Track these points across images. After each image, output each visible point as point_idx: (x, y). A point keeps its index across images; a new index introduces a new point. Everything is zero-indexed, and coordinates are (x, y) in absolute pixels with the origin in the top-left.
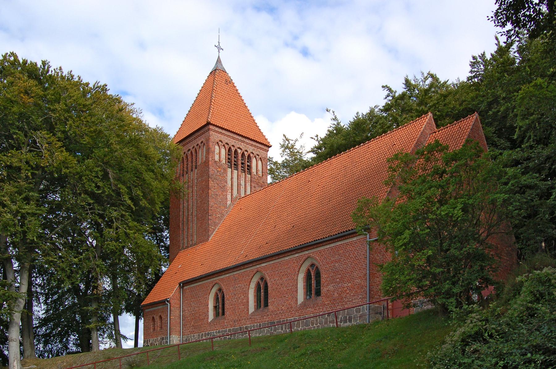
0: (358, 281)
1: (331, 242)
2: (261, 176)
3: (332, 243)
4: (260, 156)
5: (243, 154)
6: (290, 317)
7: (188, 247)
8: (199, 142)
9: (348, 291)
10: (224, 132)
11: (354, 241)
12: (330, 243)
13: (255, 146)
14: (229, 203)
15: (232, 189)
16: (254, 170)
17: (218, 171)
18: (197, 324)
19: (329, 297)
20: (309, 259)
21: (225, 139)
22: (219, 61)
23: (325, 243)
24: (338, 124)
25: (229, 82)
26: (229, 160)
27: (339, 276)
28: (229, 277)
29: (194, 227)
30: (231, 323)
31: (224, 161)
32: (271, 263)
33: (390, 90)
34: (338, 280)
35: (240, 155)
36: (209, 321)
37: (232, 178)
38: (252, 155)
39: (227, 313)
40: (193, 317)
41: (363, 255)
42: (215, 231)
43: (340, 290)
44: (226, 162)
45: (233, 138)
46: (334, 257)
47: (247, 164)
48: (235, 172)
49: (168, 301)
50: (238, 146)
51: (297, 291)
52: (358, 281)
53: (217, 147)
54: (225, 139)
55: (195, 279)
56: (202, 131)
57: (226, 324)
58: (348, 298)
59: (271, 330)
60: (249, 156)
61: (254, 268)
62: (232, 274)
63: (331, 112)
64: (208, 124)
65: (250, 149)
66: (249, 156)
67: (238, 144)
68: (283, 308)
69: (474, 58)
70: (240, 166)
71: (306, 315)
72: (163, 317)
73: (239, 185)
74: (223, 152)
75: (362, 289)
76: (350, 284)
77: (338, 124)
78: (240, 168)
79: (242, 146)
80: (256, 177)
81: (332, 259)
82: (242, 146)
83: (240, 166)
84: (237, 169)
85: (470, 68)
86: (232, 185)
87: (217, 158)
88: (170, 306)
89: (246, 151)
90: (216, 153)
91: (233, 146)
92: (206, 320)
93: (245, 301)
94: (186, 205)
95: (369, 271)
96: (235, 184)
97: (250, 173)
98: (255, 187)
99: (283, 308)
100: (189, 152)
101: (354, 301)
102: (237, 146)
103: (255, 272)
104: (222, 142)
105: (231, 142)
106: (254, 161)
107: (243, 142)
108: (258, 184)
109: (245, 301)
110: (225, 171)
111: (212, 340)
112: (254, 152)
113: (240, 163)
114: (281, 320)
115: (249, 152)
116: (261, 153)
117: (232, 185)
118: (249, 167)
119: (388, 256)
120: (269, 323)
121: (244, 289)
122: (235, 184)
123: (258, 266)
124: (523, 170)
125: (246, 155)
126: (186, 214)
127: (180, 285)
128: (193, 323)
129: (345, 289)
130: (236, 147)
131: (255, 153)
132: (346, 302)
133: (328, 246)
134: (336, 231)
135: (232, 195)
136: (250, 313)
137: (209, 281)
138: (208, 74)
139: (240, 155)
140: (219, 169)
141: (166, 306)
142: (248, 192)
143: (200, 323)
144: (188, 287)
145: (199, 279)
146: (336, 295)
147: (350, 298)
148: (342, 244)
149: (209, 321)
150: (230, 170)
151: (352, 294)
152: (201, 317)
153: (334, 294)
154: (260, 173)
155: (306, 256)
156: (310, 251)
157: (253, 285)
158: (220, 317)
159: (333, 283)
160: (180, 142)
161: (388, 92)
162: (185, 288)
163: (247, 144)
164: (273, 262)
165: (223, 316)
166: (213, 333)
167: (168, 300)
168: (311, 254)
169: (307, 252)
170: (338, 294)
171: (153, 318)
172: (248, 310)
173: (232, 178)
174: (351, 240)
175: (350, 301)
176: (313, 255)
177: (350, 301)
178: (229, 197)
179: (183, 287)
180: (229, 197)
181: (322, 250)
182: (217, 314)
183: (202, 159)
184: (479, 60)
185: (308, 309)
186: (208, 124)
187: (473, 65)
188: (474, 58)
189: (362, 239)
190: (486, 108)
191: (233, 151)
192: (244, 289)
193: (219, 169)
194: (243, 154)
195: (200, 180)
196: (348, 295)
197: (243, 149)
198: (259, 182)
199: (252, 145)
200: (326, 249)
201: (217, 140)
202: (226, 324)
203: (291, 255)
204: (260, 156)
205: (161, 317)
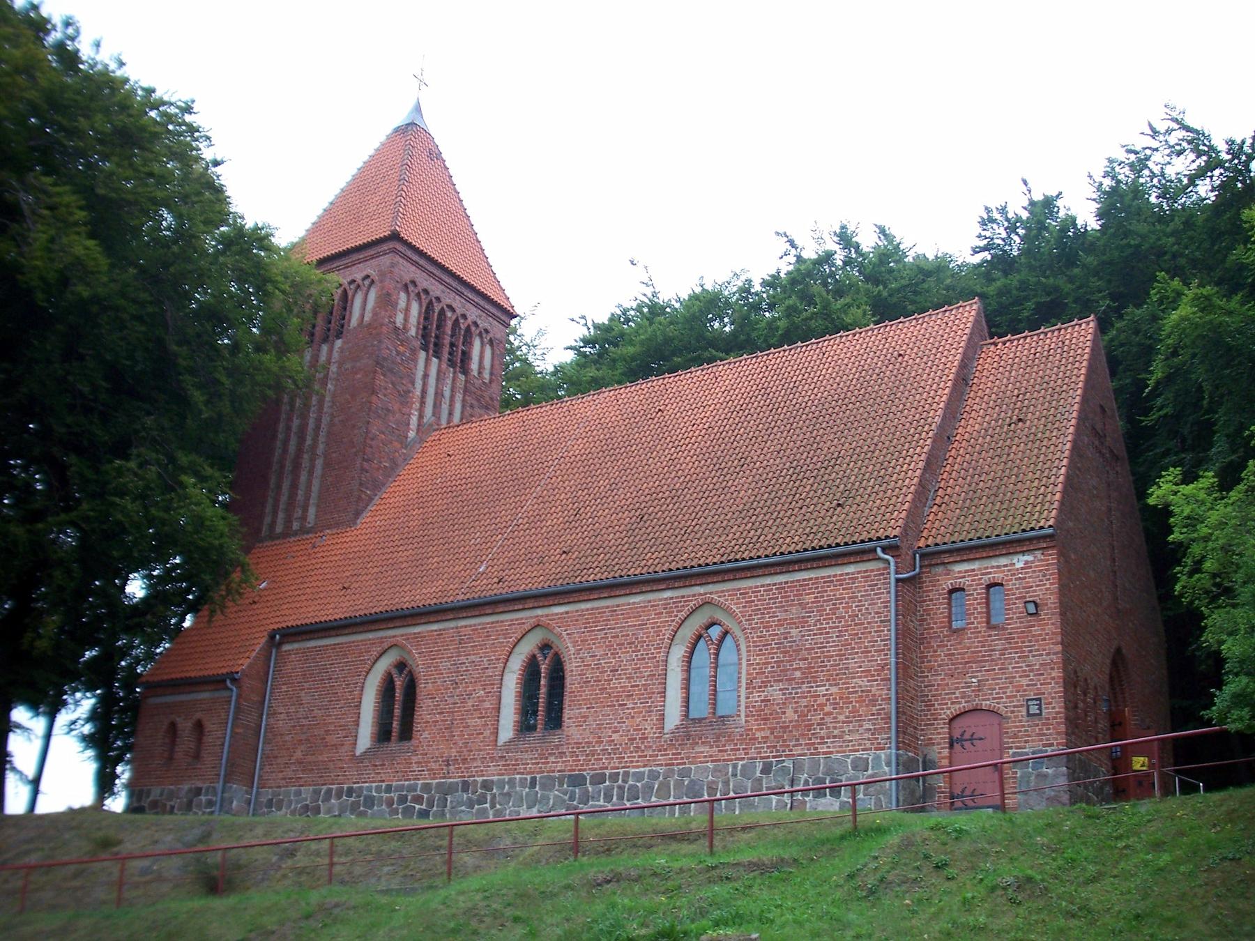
0: (862, 682)
1: (778, 569)
2: (487, 381)
3: (781, 573)
4: (491, 335)
5: (456, 322)
6: (638, 767)
7: (285, 535)
8: (358, 277)
9: (828, 708)
10: (422, 262)
11: (847, 574)
12: (776, 574)
13: (483, 309)
14: (412, 434)
15: (423, 403)
16: (474, 366)
17: (398, 353)
18: (310, 758)
19: (768, 719)
20: (706, 609)
21: (424, 282)
22: (418, 109)
23: (760, 572)
24: (655, 294)
25: (435, 155)
26: (425, 332)
27: (802, 665)
28: (440, 633)
29: (313, 482)
30: (434, 766)
31: (413, 332)
32: (583, 606)
33: (792, 244)
34: (798, 674)
35: (449, 323)
36: (358, 753)
37: (426, 376)
38: (473, 328)
39: (424, 733)
40: (304, 737)
41: (877, 613)
42: (374, 502)
43: (804, 702)
44: (417, 333)
45: (441, 281)
46: (786, 611)
47: (461, 347)
48: (435, 360)
49: (234, 680)
50: (448, 301)
51: (663, 693)
52: (862, 682)
53: (403, 296)
54: (424, 282)
55: (324, 625)
56: (371, 252)
57: (415, 767)
58: (828, 728)
59: (572, 798)
60: (468, 329)
61: (529, 616)
62: (452, 624)
63: (640, 266)
64: (395, 236)
65: (473, 314)
66: (468, 329)
67: (449, 298)
68: (615, 736)
69: (988, 210)
70: (446, 349)
71: (691, 763)
72: (209, 726)
73: (439, 394)
74: (415, 309)
75: (875, 705)
76: (834, 690)
77: (655, 294)
78: (446, 356)
79: (457, 302)
80: (478, 383)
81: (781, 616)
82: (457, 302)
83: (446, 349)
84: (437, 354)
85: (978, 229)
86: (424, 392)
87: (399, 319)
88: (239, 696)
89: (464, 316)
90: (399, 307)
91: (438, 299)
92: (346, 748)
93: (487, 705)
94: (296, 423)
95: (897, 658)
96: (431, 391)
97: (465, 370)
98: (472, 406)
99: (615, 736)
100: (340, 291)
101: (847, 737)
102: (447, 300)
103: (527, 627)
104: (416, 286)
105: (436, 289)
106: (477, 343)
107: (461, 294)
108: (478, 401)
109: (487, 705)
110: (414, 352)
111: (577, 820)
112: (479, 322)
113: (447, 340)
114: (607, 772)
115: (469, 321)
116: (496, 330)
117: (424, 392)
118: (466, 356)
119: (936, 623)
120: (564, 776)
121: (489, 672)
122: (431, 391)
123: (539, 612)
124: (92, 513)
125: (462, 326)
126: (292, 447)
127: (272, 637)
128: (298, 754)
129: (821, 700)
130: (443, 304)
131: (482, 324)
132: (822, 738)
133: (768, 581)
134: (791, 541)
135: (421, 417)
136: (500, 742)
137: (370, 636)
138: (389, 130)
139: (449, 323)
140: (401, 349)
141: (225, 694)
142: (456, 418)
143: (324, 757)
144: (296, 646)
145: (362, 623)
146: (790, 714)
147: (835, 728)
148: (811, 579)
149: (358, 753)
150: (422, 355)
151: (841, 718)
152: (332, 739)
153: (784, 713)
154: (486, 375)
155: (700, 600)
156: (710, 588)
157: (516, 664)
158: (394, 745)
159: (781, 681)
160: (322, 262)
161: (788, 245)
162: (286, 647)
163: (469, 301)
164: (589, 605)
165: (406, 744)
166: (370, 789)
167: (236, 676)
168: (715, 597)
169: (701, 590)
170: (796, 712)
171: (173, 726)
172: (496, 733)
173: (426, 376)
174: (838, 571)
175: (835, 737)
176: (722, 600)
177: (835, 737)
178: (414, 420)
179: (280, 644)
180: (414, 420)
181: (751, 588)
182: (383, 734)
183: (362, 316)
184: (996, 215)
185: (698, 749)
186: (395, 236)
187: (986, 222)
188: (988, 210)
189: (872, 571)
190: (1032, 315)
191: (437, 310)
192: (489, 672)
193: (401, 349)
194: (456, 322)
195: (348, 366)
196: (828, 719)
197: (459, 311)
198: (482, 396)
199: (477, 305)
200: (763, 586)
201: (407, 278)
202: (415, 767)
203: (652, 591)
204: (491, 335)
205: (199, 726)
